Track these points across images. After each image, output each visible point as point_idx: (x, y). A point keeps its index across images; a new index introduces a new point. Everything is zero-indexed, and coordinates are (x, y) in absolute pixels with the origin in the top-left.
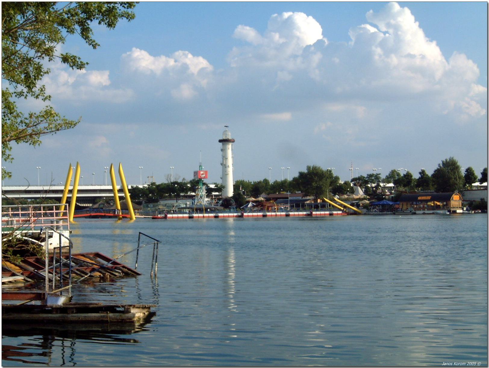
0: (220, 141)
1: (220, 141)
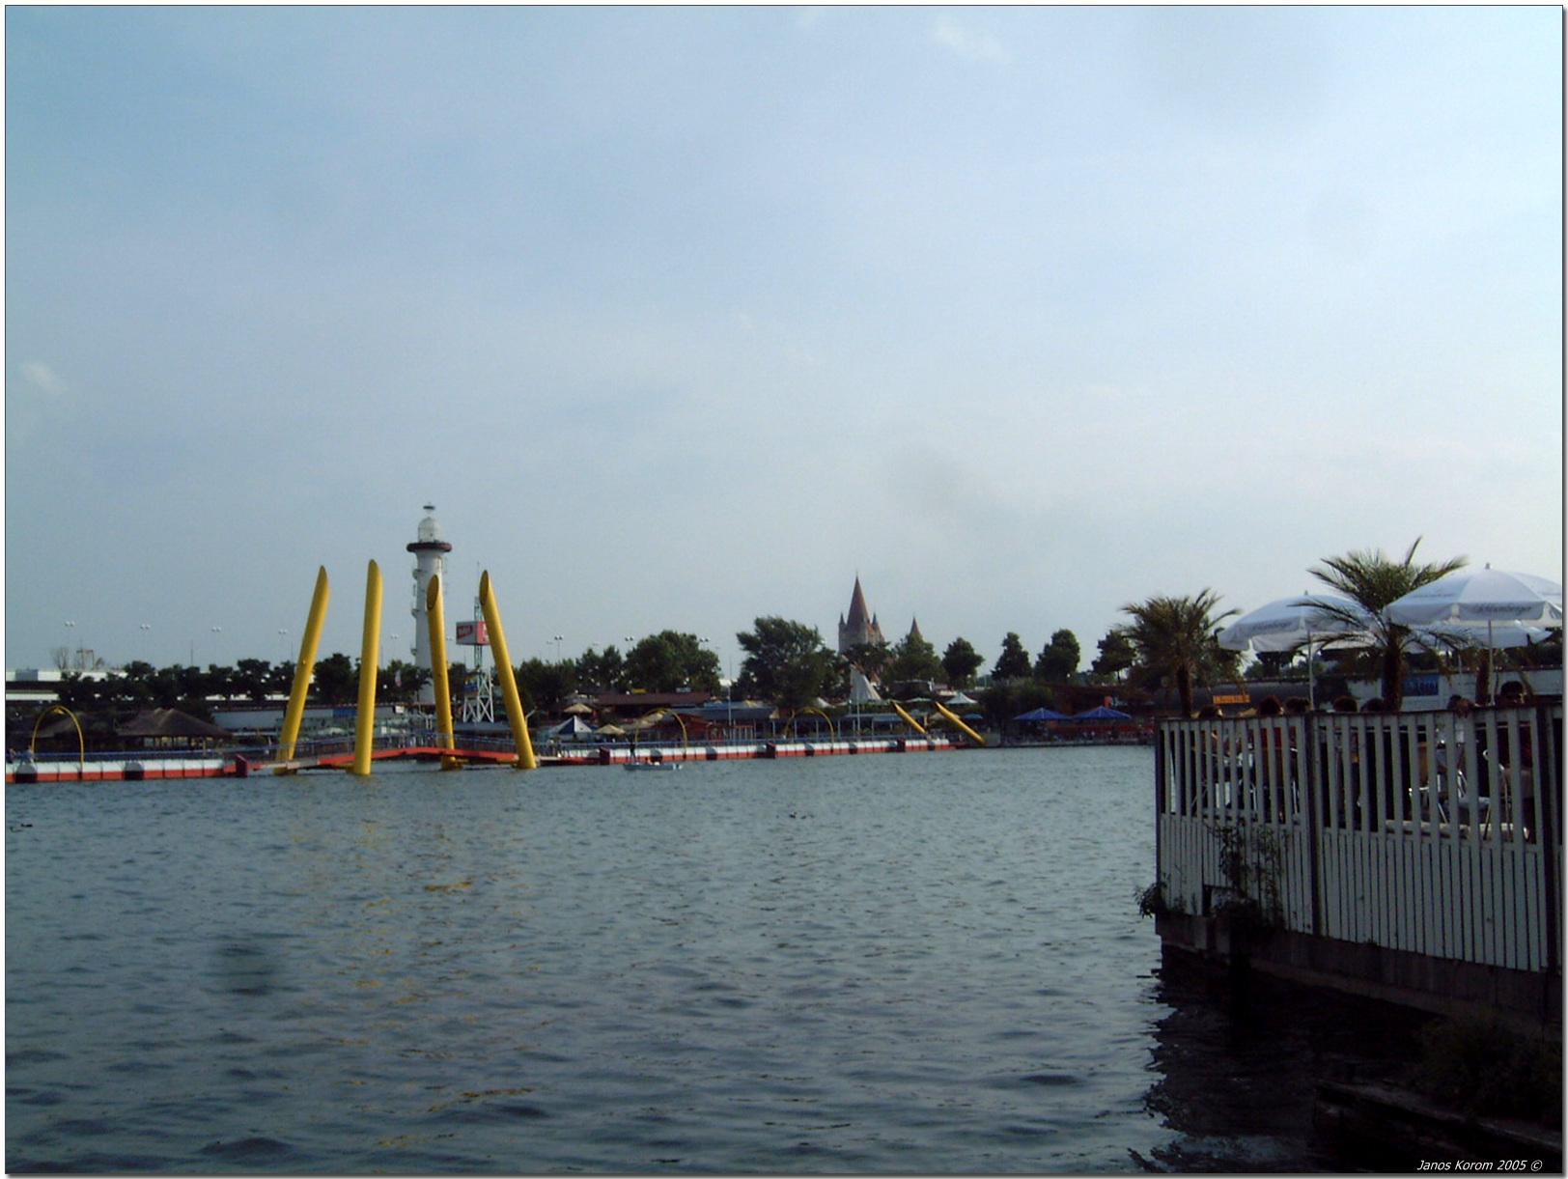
0: (411, 548)
1: (411, 548)
